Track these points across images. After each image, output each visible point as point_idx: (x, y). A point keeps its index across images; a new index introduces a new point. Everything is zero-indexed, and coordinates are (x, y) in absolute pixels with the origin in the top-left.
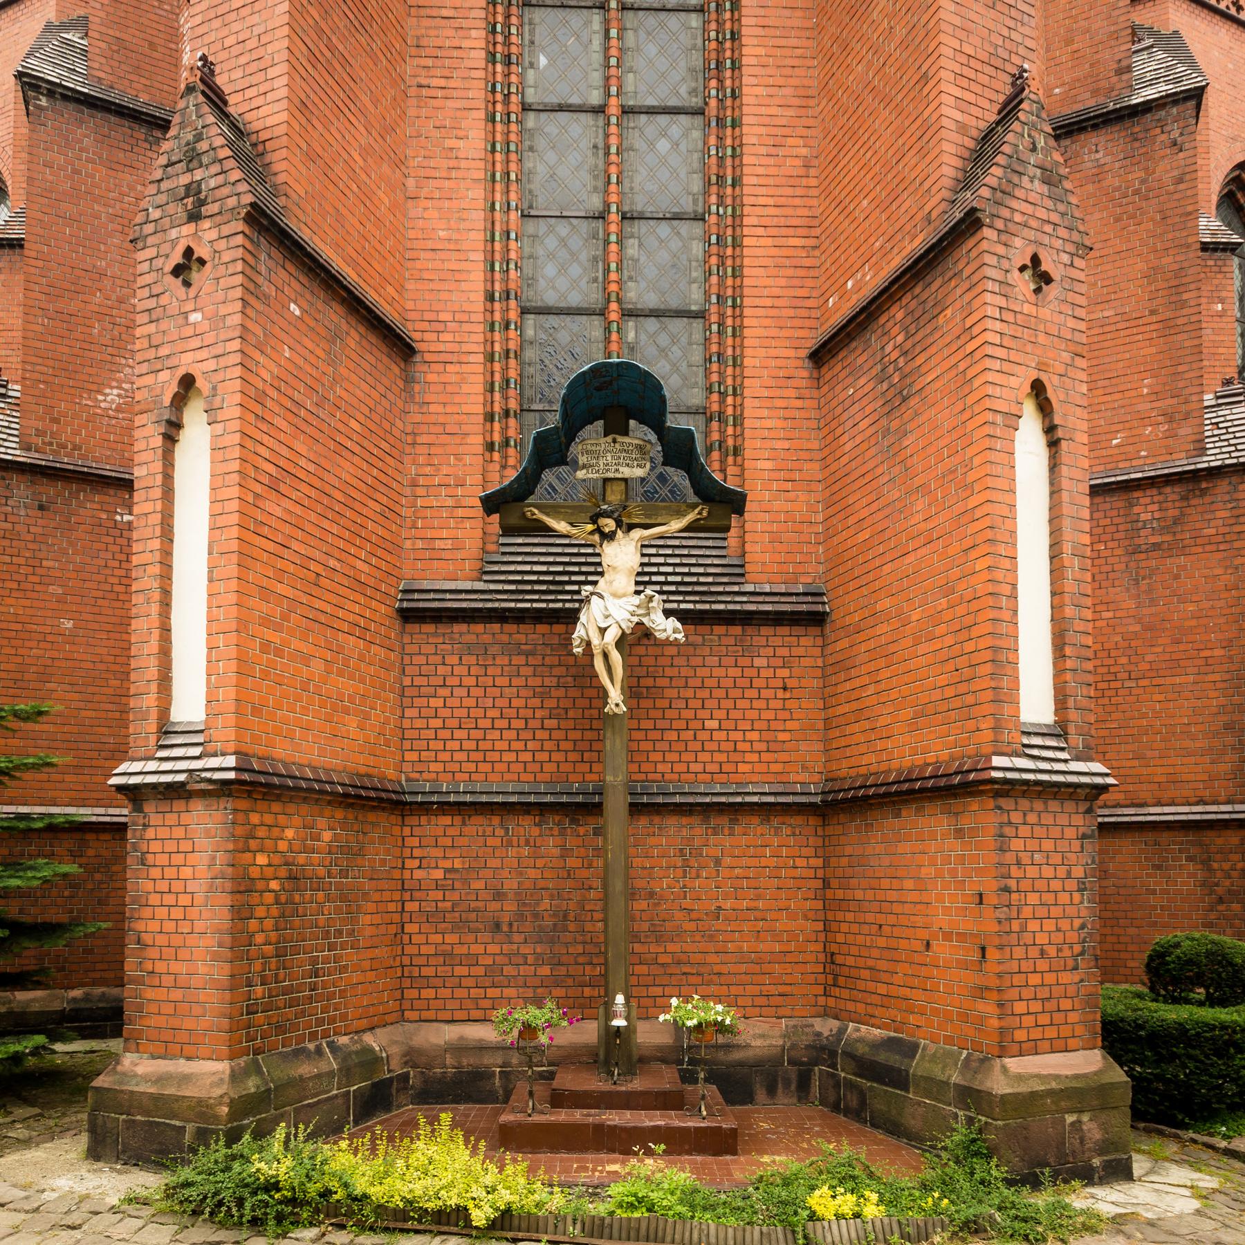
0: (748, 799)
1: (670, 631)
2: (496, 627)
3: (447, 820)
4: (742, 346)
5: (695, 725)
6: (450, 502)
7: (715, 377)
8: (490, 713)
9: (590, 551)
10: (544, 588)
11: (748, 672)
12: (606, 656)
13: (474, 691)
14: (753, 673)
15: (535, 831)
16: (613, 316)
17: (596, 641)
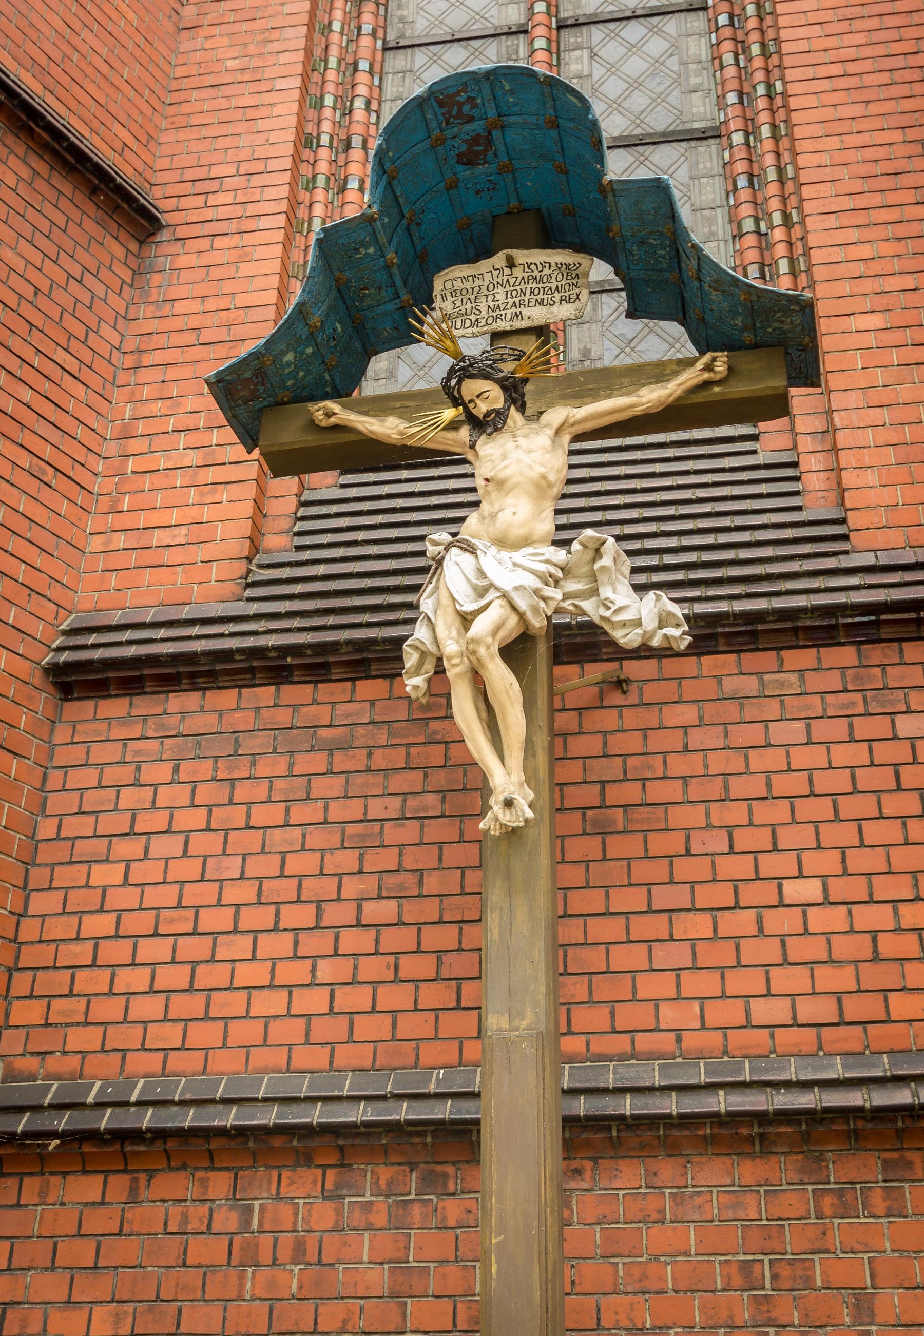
1: (650, 624)
2: (265, 694)
3: (89, 1187)
6: (193, 458)
8: (233, 894)
12: (477, 679)
15: (324, 1214)
17: (451, 647)
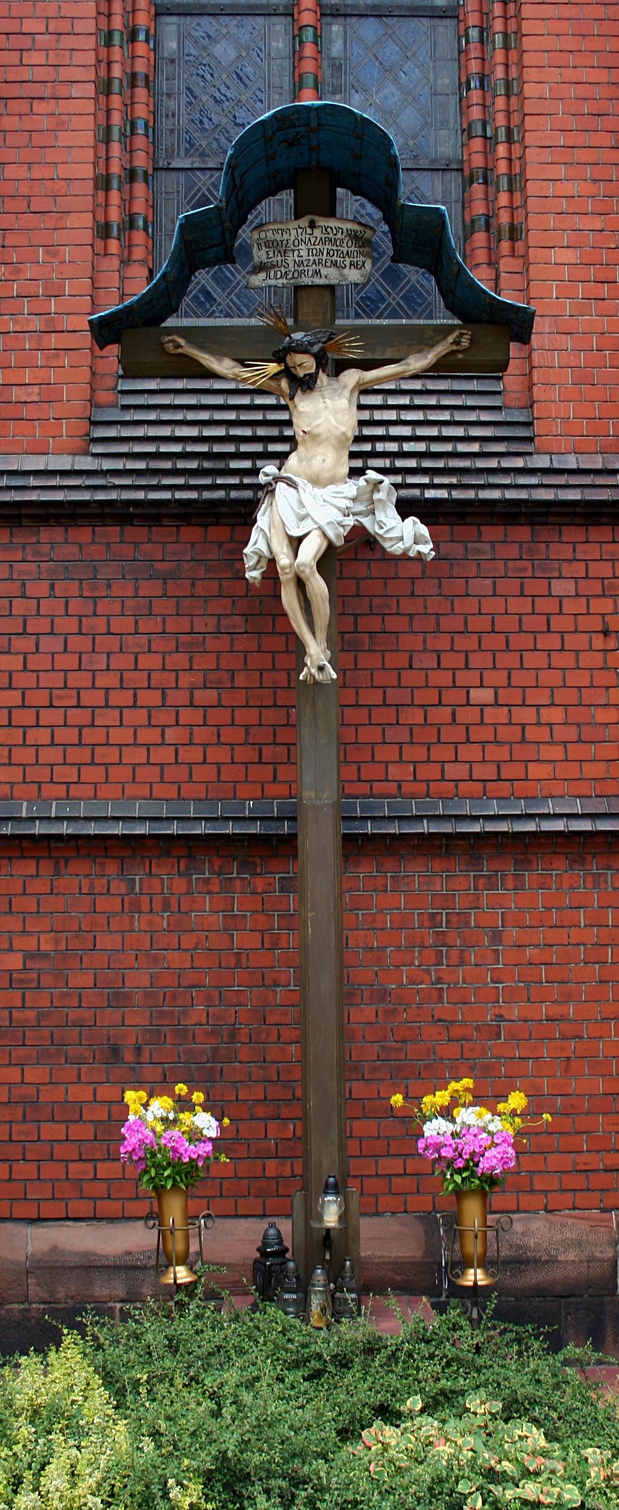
0: (548, 826)
1: (408, 541)
2: (113, 532)
4: (522, 67)
5: (451, 696)
6: (37, 324)
7: (476, 113)
8: (103, 680)
9: (270, 401)
10: (193, 465)
11: (543, 605)
12: (300, 584)
13: (76, 643)
14: (551, 606)
15: (180, 885)
16: (307, 18)
17: (284, 560)
